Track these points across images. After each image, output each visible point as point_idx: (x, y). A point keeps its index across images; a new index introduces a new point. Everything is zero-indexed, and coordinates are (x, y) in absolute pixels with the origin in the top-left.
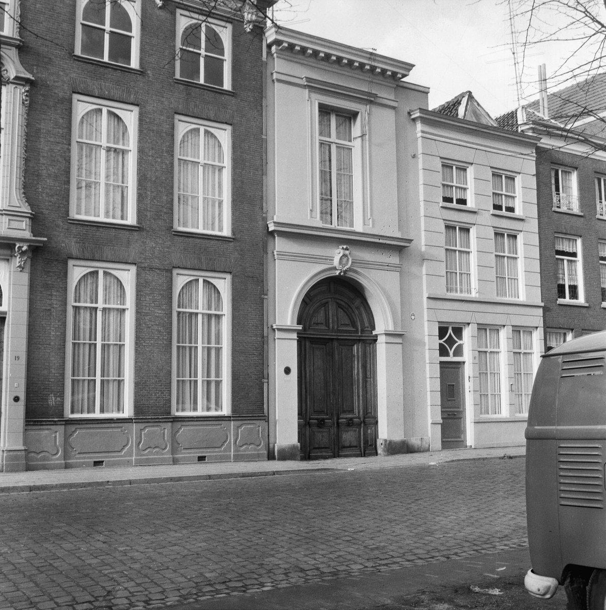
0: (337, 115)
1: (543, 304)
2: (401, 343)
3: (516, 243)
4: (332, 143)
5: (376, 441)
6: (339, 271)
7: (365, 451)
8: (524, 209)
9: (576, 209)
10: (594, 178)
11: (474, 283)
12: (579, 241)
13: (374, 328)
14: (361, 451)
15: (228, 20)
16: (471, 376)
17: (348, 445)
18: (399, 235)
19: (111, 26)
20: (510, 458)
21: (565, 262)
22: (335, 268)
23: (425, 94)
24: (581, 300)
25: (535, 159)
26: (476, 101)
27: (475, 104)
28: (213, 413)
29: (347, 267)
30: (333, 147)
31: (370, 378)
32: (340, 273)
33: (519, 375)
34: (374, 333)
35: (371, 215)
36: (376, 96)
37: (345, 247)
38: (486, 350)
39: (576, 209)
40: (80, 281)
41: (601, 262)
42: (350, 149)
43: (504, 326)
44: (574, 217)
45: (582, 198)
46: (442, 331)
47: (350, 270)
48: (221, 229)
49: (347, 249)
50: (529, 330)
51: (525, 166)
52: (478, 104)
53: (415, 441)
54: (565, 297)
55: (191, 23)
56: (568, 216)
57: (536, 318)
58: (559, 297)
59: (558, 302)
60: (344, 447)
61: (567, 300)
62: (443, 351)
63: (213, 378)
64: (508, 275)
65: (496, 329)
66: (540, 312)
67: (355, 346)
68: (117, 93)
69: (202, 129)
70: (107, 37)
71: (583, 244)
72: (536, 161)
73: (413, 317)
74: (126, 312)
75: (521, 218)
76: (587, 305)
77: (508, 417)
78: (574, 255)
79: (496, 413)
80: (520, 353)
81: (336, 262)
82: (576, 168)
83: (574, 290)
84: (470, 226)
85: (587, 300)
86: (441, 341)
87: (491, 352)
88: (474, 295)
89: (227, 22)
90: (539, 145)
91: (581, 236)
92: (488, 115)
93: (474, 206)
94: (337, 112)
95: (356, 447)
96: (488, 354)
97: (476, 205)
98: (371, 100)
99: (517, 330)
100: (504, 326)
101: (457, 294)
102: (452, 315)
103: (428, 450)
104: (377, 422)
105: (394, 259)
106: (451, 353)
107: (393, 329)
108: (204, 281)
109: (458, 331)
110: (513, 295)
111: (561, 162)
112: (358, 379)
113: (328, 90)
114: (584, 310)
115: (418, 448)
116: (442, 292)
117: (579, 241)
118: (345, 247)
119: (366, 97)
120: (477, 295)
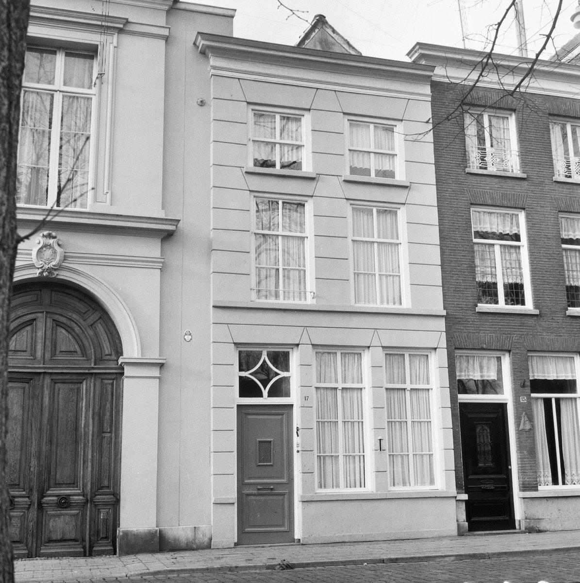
0: (67, 55)
1: (444, 313)
2: (159, 378)
3: (396, 220)
4: (56, 91)
5: (115, 531)
6: (40, 270)
7: (91, 547)
8: (408, 172)
9: (514, 165)
10: (539, 119)
11: (311, 284)
12: (522, 216)
13: (119, 352)
14: (84, 547)
16: (300, 427)
17: (59, 538)
18: (161, 215)
20: (289, 567)
21: (497, 249)
22: (32, 266)
23: (229, 19)
24: (529, 306)
25: (430, 99)
26: (331, 27)
27: (329, 31)
29: (54, 263)
30: (58, 97)
31: (111, 432)
32: (41, 273)
33: (404, 425)
34: (120, 361)
35: (110, 186)
36: (127, 22)
37: (46, 233)
38: (333, 385)
39: (514, 165)
41: (564, 246)
42: (88, 98)
43: (298, 345)
44: (509, 181)
45: (524, 154)
46: (247, 359)
47: (59, 267)
49: (50, 236)
50: (422, 353)
52: (334, 31)
53: (180, 531)
54: (497, 302)
56: (496, 180)
57: (435, 334)
58: (569, 306)
59: (477, 309)
60: (50, 541)
61: (502, 305)
62: (247, 388)
64: (380, 270)
65: (353, 351)
66: (441, 324)
67: (84, 383)
71: (528, 220)
72: (432, 101)
73: (188, 338)
75: (311, 176)
76: (537, 312)
77: (375, 492)
78: (517, 237)
79: (355, 487)
80: (405, 389)
82: (514, 110)
83: (515, 293)
84: (306, 199)
85: (536, 306)
86: (283, 374)
87: (343, 388)
88: (309, 302)
90: (434, 79)
91: (524, 209)
92: (348, 43)
93: (404, 179)
94: (67, 49)
95: (75, 540)
96: (339, 393)
97: (314, 169)
99: (394, 353)
100: (298, 345)
101: (277, 301)
102: (265, 333)
103: (209, 546)
104: (117, 501)
105: (151, 249)
106: (265, 392)
107: (140, 356)
109: (281, 359)
110: (391, 299)
111: (482, 102)
112: (86, 433)
113: (365, 68)
114: (531, 322)
115: (187, 545)
118: (46, 233)
119: (99, 23)
120: (314, 301)
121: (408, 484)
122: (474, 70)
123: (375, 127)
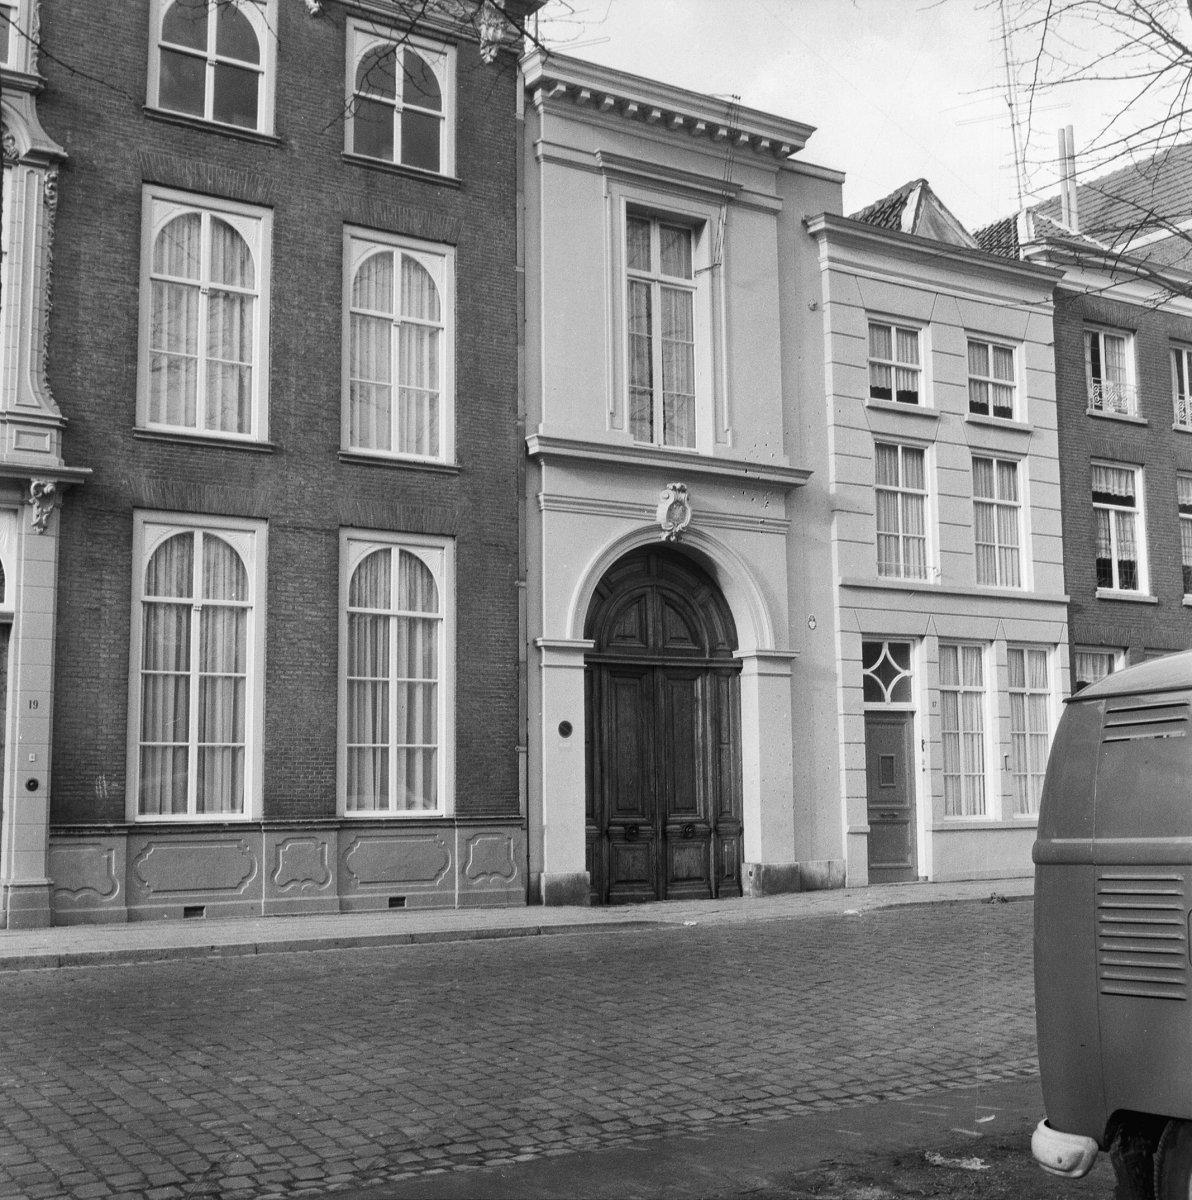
0: (662, 227)
1: (1067, 599)
2: (790, 676)
3: (1015, 477)
4: (654, 281)
5: (739, 868)
6: (667, 534)
7: (717, 887)
8: (1031, 411)
9: (1132, 410)
10: (1169, 351)
11: (933, 558)
12: (1139, 475)
13: (735, 646)
14: (710, 888)
15: (449, 40)
16: (927, 739)
17: (685, 875)
18: (784, 462)
19: (219, 51)
20: (1004, 900)
21: (1112, 515)
22: (659, 528)
23: (836, 185)
24: (1144, 590)
25: (1052, 313)
26: (936, 198)
27: (935, 204)
28: (418, 813)
29: (683, 525)
30: (656, 290)
31: (728, 744)
32: (668, 538)
33: (1021, 738)
34: (736, 655)
35: (730, 423)
36: (739, 188)
37: (678, 485)
38: (955, 688)
39: (1132, 410)
40: (156, 554)
41: (1182, 515)
42: (687, 293)
43: (992, 641)
44: (1129, 427)
45: (1145, 390)
46: (870, 652)
47: (688, 530)
48: (434, 451)
49: (682, 490)
50: (1040, 649)
51: (1033, 326)
52: (941, 205)
53: (816, 868)
54: (1110, 585)
55: (376, 44)
56: (1117, 426)
57: (1055, 625)
58: (1100, 585)
59: (1097, 595)
60: (677, 880)
61: (1116, 590)
62: (872, 691)
63: (419, 743)
64: (999, 542)
65: (975, 646)
66: (1062, 613)
67: (699, 681)
68: (230, 184)
69: (397, 254)
70: (210, 73)
71: (1147, 480)
72: (1054, 317)
73: (812, 624)
74: (249, 613)
75: (1025, 428)
76: (1154, 600)
77: (1000, 819)
78: (1129, 501)
79: (975, 813)
80: (1022, 694)
81: (661, 516)
82: (1134, 331)
83: (1128, 570)
84: (925, 444)
85: (1155, 590)
86: (868, 672)
87: (966, 692)
88: (932, 580)
89: (446, 42)
90: (1059, 285)
91: (1142, 465)
92: (961, 226)
93: (932, 405)
94: (663, 219)
95: (700, 879)
96: (959, 696)
97: (936, 404)
98: (729, 197)
99: (1016, 649)
100: (992, 641)
101: (898, 579)
102: (889, 619)
103: (842, 885)
104: (741, 830)
105: (775, 510)
106: (888, 694)
107: (773, 648)
108: (402, 552)
109: (901, 652)
110: (1010, 580)
111: (1103, 319)
112: (705, 746)
114: (1149, 611)
115: (822, 882)
116: (869, 575)
117: (1139, 475)
118: (678, 485)
119: (719, 192)
120: (939, 579)
121: (238, 810)
122: (28, 38)
123: (662, 288)
